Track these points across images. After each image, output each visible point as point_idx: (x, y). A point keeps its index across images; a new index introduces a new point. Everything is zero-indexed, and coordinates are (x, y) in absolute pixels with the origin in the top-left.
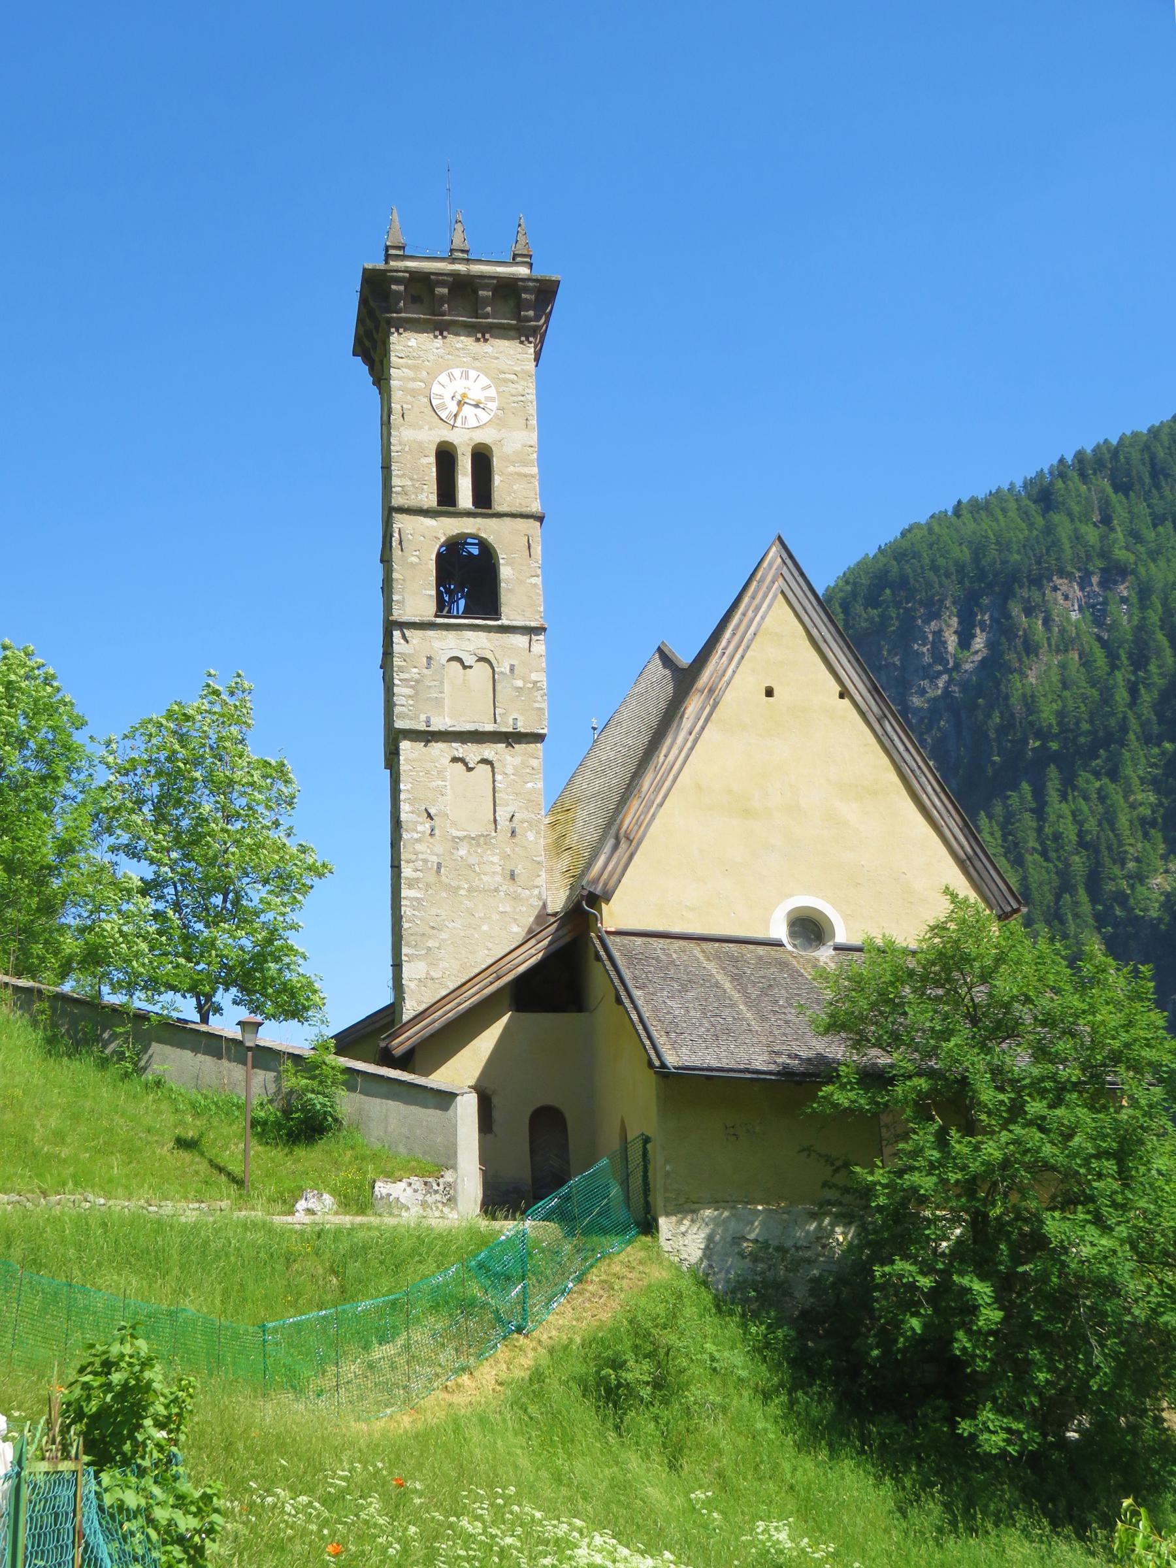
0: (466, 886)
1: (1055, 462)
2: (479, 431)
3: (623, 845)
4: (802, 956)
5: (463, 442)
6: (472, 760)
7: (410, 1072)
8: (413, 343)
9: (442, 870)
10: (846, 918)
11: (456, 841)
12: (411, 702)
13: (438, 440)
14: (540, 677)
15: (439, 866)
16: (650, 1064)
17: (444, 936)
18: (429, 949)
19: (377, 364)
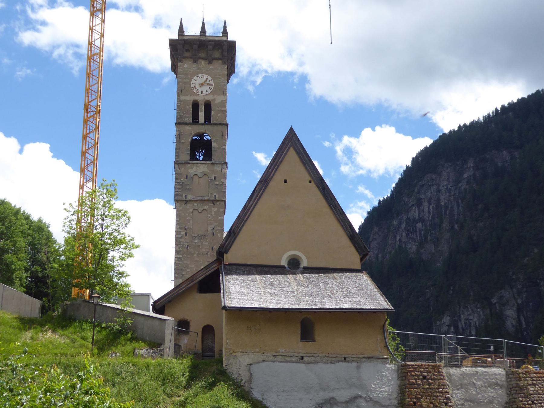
0: (197, 253)
1: (494, 110)
3: (232, 235)
5: (201, 99)
8: (186, 66)
9: (189, 247)
10: (308, 258)
11: (194, 238)
15: (188, 246)
17: (188, 270)
18: (183, 275)
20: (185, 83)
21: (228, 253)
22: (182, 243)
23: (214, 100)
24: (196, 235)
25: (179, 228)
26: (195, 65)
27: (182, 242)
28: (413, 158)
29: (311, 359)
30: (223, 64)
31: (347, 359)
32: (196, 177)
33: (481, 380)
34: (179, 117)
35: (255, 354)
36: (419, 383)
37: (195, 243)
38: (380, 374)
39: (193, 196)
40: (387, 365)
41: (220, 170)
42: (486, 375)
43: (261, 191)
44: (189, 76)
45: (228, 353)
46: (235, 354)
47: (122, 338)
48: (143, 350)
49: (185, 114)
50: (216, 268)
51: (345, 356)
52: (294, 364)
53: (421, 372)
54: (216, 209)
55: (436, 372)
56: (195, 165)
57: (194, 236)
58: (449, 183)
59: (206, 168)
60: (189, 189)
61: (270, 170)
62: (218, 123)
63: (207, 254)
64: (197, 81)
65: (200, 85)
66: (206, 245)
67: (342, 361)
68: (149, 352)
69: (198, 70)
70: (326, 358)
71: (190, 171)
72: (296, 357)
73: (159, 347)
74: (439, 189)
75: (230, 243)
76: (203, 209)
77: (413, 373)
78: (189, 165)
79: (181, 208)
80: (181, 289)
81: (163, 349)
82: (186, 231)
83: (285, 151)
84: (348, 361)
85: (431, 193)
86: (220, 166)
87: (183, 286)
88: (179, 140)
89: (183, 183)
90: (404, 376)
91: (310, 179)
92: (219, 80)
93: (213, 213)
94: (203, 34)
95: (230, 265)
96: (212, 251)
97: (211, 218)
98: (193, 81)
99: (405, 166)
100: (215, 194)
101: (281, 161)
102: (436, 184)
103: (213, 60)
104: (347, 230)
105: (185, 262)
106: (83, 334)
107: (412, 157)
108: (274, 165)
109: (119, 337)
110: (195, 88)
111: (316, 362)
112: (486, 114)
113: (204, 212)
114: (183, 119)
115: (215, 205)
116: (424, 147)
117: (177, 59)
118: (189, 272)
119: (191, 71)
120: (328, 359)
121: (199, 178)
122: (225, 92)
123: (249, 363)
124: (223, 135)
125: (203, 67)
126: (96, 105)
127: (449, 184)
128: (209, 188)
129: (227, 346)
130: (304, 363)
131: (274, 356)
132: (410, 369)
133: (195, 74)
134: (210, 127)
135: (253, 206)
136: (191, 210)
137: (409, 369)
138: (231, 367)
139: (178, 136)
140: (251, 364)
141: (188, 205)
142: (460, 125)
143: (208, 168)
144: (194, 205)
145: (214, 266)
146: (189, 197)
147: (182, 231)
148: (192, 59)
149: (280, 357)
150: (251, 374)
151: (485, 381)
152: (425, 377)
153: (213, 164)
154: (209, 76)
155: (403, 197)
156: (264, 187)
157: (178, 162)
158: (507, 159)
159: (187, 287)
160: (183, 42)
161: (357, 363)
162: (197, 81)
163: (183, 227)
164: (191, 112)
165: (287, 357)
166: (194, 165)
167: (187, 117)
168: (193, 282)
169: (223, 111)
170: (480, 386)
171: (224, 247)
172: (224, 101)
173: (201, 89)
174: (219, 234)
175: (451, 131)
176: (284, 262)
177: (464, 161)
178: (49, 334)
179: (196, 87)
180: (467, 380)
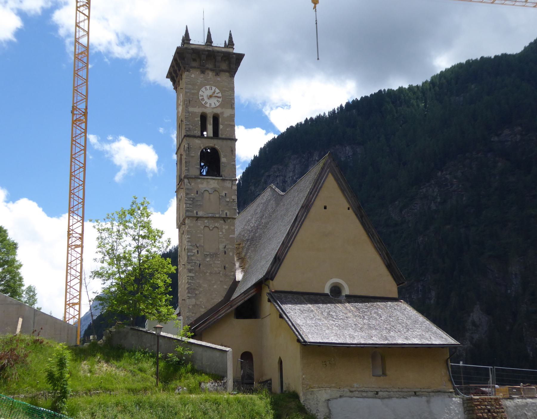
0: (209, 272)
1: (339, 106)
2: (215, 109)
4: (336, 300)
5: (209, 111)
6: (211, 226)
7: (201, 340)
8: (193, 76)
9: (201, 266)
10: (349, 286)
11: (206, 256)
16: (298, 341)
17: (201, 289)
18: (196, 294)
21: (274, 280)
23: (222, 113)
26: (202, 76)
27: (194, 260)
28: (261, 149)
29: (385, 394)
30: (230, 77)
31: (417, 394)
33: (530, 410)
34: (188, 129)
35: (331, 389)
36: (485, 416)
37: (207, 261)
38: (448, 408)
40: (453, 399)
42: (534, 406)
43: (303, 217)
44: (197, 87)
45: (305, 389)
46: (312, 390)
47: (183, 370)
48: (209, 385)
49: (194, 126)
50: (254, 293)
51: (416, 391)
52: (371, 400)
53: (486, 406)
54: (227, 227)
55: (498, 405)
57: (206, 255)
58: (295, 175)
59: (217, 184)
60: (199, 205)
61: (311, 196)
63: (219, 273)
64: (205, 92)
65: (209, 97)
66: (218, 264)
67: (413, 396)
68: (214, 385)
69: (205, 81)
70: (399, 393)
71: (200, 186)
72: (371, 392)
73: (223, 380)
74: (285, 179)
75: (276, 270)
76: (214, 226)
77: (479, 407)
78: (199, 180)
79: (192, 225)
80: (220, 315)
81: (226, 382)
83: (324, 177)
84: (418, 396)
86: (230, 182)
87: (223, 311)
89: (194, 199)
90: (471, 410)
91: (348, 206)
93: (224, 231)
97: (222, 236)
98: (201, 93)
99: (253, 156)
100: (226, 211)
101: (321, 187)
102: (282, 175)
103: (220, 71)
104: (384, 258)
105: (198, 281)
106: (140, 365)
108: (314, 190)
109: (179, 369)
110: (203, 99)
111: (390, 397)
112: (331, 110)
113: (215, 229)
115: (226, 222)
116: (272, 139)
117: (185, 68)
118: (201, 291)
119: (199, 81)
120: (400, 393)
121: (209, 194)
122: (233, 106)
123: (327, 399)
124: (232, 151)
125: (211, 79)
126: (85, 108)
127: (294, 176)
128: (219, 204)
129: (304, 381)
130: (379, 398)
131: (351, 391)
132: (476, 403)
133: (202, 85)
135: (295, 233)
136: (202, 227)
137: (475, 403)
138: (309, 403)
140: (329, 400)
141: (199, 222)
142: (307, 119)
143: (218, 184)
144: (205, 222)
145: (252, 291)
146: (200, 214)
147: (193, 248)
149: (357, 392)
150: (330, 410)
151: (534, 412)
152: (489, 411)
153: (223, 180)
156: (305, 213)
158: (350, 154)
159: (227, 312)
161: (426, 398)
162: (205, 92)
163: (195, 244)
164: (200, 124)
165: (364, 393)
166: (205, 180)
167: (196, 130)
168: (231, 307)
170: (531, 417)
171: (270, 274)
172: (233, 115)
173: (209, 102)
175: (298, 124)
176: (327, 291)
177: (309, 154)
178: (105, 366)
180: (520, 411)
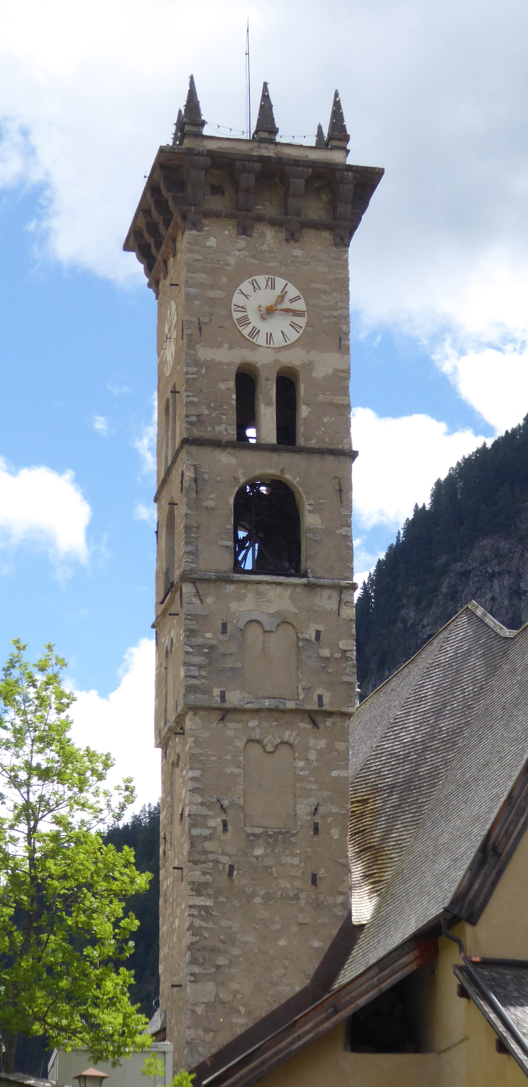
0: (262, 892)
3: (491, 860)
6: (270, 740)
8: (212, 242)
9: (235, 873)
12: (203, 673)
13: (238, 361)
14: (349, 645)
15: (232, 868)
17: (235, 951)
18: (218, 967)
19: (158, 265)
20: (213, 302)
22: (211, 857)
24: (259, 831)
25: (202, 804)
26: (242, 242)
27: (212, 853)
28: (438, 484)
30: (336, 245)
32: (254, 631)
34: (194, 419)
37: (257, 857)
39: (246, 695)
41: (335, 607)
44: (225, 280)
49: (214, 409)
54: (322, 744)
56: (252, 587)
57: (253, 835)
62: (323, 446)
66: (293, 866)
71: (234, 606)
75: (485, 890)
76: (279, 741)
78: (231, 588)
79: (206, 735)
82: (223, 817)
85: (493, 599)
86: (335, 594)
88: (197, 499)
89: (212, 648)
92: (325, 298)
93: (312, 756)
94: (264, 135)
95: (487, 963)
96: (313, 887)
97: (307, 772)
98: (237, 299)
100: (320, 691)
102: (509, 572)
105: (224, 923)
107: (435, 480)
110: (245, 321)
113: (284, 750)
114: (209, 429)
117: (184, 217)
118: (237, 957)
119: (232, 260)
121: (265, 632)
122: (343, 343)
124: (340, 491)
125: (270, 252)
128: (298, 668)
134: (298, 460)
136: (240, 744)
139: (194, 486)
141: (231, 725)
143: (292, 599)
147: (211, 813)
148: (234, 222)
153: (310, 586)
154: (289, 285)
155: (403, 606)
157: (196, 576)
160: (209, 160)
163: (214, 800)
164: (234, 403)
166: (249, 586)
167: (220, 422)
168: (336, 1012)
169: (338, 406)
172: (343, 371)
173: (264, 327)
174: (333, 831)
179: (249, 316)
